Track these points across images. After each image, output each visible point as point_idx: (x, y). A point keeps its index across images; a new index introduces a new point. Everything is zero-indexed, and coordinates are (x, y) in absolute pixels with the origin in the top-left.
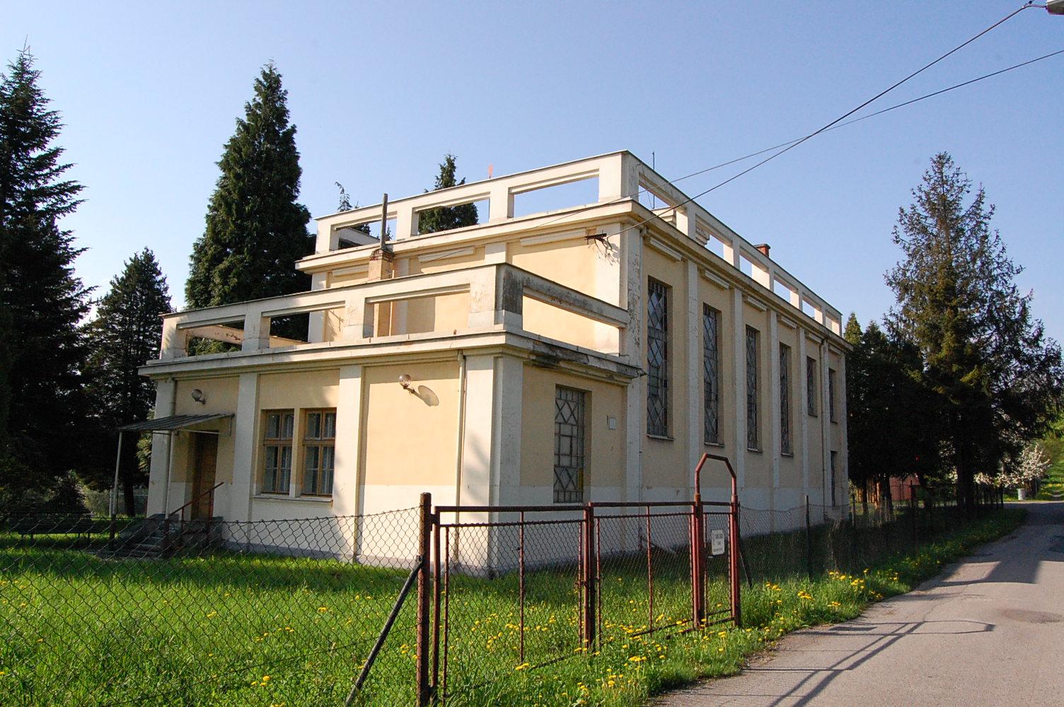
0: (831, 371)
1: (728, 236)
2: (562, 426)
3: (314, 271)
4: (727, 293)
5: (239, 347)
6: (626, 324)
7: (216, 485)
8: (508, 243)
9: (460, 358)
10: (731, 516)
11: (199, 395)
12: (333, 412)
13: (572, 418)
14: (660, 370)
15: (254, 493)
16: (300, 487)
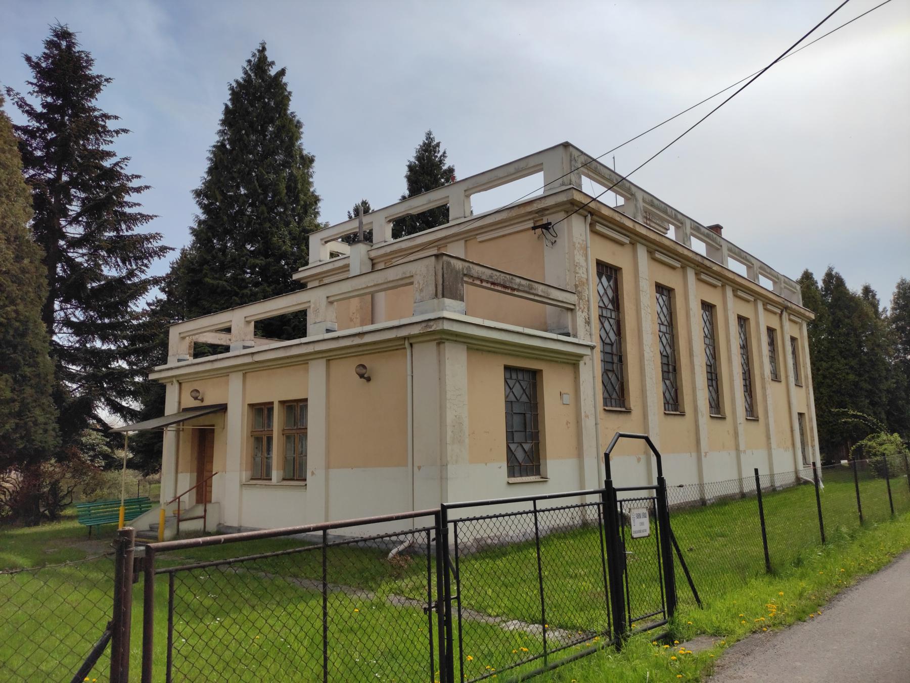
0: (793, 339)
1: (678, 219)
2: (514, 405)
3: (309, 279)
4: (719, 290)
5: (227, 349)
6: (574, 305)
7: (213, 473)
8: (466, 241)
9: (407, 345)
10: (656, 500)
11: (198, 394)
12: (271, 406)
13: (524, 397)
14: (615, 345)
15: (244, 481)
16: (281, 472)
